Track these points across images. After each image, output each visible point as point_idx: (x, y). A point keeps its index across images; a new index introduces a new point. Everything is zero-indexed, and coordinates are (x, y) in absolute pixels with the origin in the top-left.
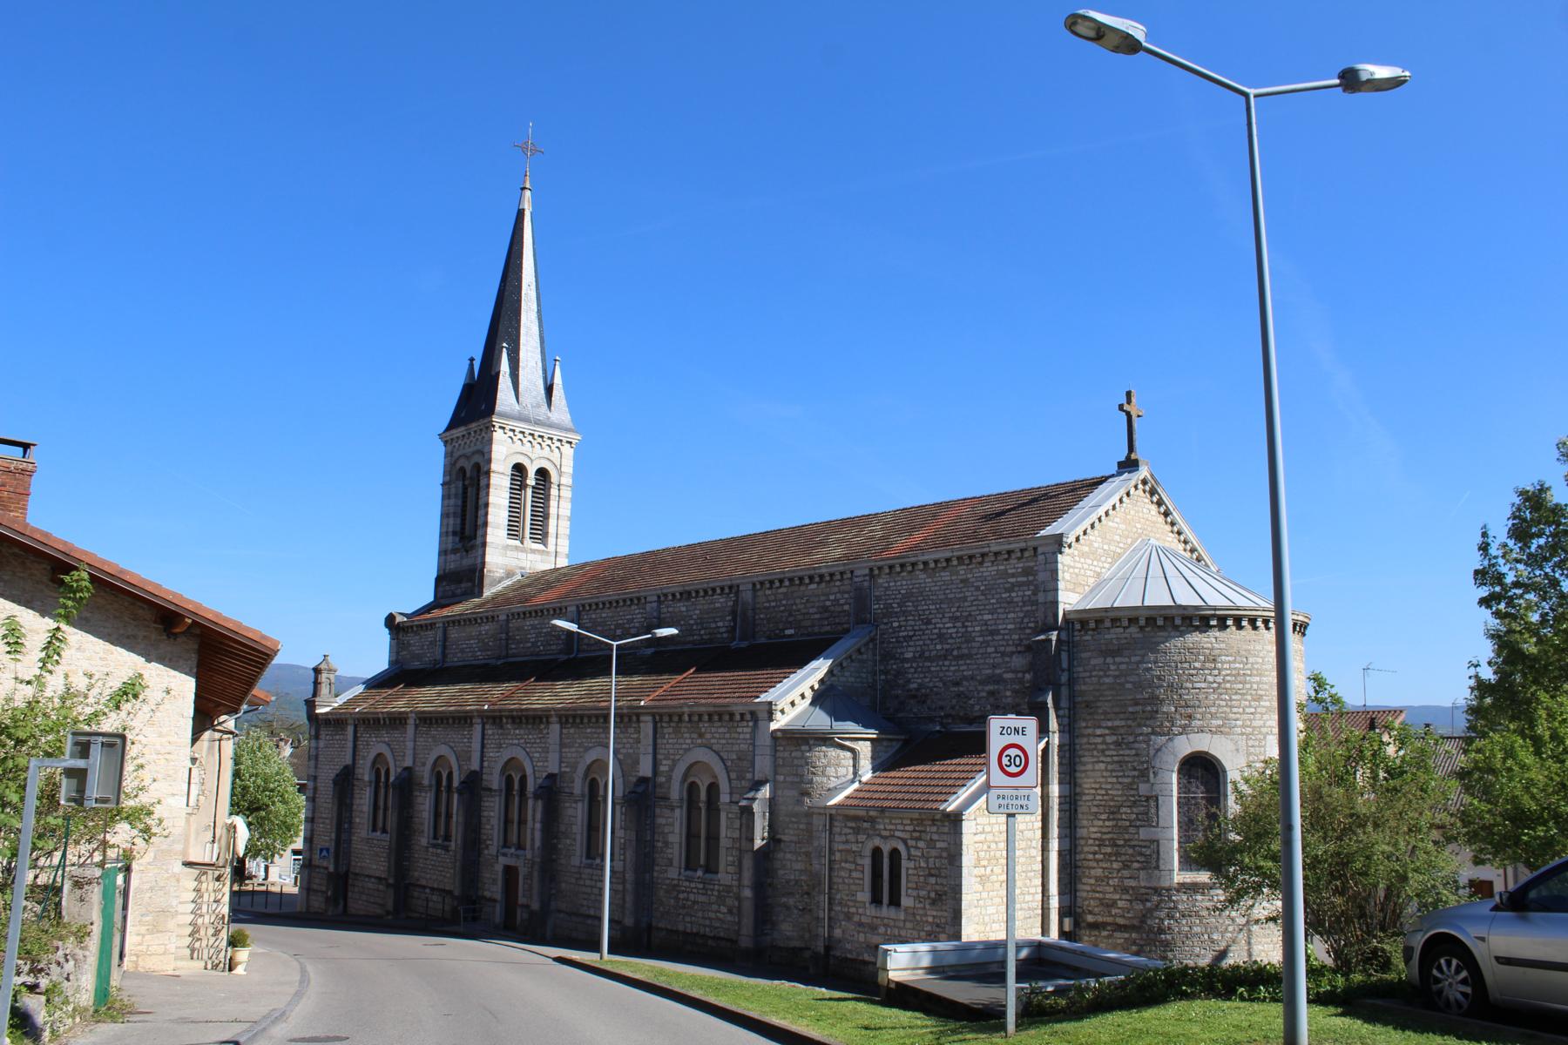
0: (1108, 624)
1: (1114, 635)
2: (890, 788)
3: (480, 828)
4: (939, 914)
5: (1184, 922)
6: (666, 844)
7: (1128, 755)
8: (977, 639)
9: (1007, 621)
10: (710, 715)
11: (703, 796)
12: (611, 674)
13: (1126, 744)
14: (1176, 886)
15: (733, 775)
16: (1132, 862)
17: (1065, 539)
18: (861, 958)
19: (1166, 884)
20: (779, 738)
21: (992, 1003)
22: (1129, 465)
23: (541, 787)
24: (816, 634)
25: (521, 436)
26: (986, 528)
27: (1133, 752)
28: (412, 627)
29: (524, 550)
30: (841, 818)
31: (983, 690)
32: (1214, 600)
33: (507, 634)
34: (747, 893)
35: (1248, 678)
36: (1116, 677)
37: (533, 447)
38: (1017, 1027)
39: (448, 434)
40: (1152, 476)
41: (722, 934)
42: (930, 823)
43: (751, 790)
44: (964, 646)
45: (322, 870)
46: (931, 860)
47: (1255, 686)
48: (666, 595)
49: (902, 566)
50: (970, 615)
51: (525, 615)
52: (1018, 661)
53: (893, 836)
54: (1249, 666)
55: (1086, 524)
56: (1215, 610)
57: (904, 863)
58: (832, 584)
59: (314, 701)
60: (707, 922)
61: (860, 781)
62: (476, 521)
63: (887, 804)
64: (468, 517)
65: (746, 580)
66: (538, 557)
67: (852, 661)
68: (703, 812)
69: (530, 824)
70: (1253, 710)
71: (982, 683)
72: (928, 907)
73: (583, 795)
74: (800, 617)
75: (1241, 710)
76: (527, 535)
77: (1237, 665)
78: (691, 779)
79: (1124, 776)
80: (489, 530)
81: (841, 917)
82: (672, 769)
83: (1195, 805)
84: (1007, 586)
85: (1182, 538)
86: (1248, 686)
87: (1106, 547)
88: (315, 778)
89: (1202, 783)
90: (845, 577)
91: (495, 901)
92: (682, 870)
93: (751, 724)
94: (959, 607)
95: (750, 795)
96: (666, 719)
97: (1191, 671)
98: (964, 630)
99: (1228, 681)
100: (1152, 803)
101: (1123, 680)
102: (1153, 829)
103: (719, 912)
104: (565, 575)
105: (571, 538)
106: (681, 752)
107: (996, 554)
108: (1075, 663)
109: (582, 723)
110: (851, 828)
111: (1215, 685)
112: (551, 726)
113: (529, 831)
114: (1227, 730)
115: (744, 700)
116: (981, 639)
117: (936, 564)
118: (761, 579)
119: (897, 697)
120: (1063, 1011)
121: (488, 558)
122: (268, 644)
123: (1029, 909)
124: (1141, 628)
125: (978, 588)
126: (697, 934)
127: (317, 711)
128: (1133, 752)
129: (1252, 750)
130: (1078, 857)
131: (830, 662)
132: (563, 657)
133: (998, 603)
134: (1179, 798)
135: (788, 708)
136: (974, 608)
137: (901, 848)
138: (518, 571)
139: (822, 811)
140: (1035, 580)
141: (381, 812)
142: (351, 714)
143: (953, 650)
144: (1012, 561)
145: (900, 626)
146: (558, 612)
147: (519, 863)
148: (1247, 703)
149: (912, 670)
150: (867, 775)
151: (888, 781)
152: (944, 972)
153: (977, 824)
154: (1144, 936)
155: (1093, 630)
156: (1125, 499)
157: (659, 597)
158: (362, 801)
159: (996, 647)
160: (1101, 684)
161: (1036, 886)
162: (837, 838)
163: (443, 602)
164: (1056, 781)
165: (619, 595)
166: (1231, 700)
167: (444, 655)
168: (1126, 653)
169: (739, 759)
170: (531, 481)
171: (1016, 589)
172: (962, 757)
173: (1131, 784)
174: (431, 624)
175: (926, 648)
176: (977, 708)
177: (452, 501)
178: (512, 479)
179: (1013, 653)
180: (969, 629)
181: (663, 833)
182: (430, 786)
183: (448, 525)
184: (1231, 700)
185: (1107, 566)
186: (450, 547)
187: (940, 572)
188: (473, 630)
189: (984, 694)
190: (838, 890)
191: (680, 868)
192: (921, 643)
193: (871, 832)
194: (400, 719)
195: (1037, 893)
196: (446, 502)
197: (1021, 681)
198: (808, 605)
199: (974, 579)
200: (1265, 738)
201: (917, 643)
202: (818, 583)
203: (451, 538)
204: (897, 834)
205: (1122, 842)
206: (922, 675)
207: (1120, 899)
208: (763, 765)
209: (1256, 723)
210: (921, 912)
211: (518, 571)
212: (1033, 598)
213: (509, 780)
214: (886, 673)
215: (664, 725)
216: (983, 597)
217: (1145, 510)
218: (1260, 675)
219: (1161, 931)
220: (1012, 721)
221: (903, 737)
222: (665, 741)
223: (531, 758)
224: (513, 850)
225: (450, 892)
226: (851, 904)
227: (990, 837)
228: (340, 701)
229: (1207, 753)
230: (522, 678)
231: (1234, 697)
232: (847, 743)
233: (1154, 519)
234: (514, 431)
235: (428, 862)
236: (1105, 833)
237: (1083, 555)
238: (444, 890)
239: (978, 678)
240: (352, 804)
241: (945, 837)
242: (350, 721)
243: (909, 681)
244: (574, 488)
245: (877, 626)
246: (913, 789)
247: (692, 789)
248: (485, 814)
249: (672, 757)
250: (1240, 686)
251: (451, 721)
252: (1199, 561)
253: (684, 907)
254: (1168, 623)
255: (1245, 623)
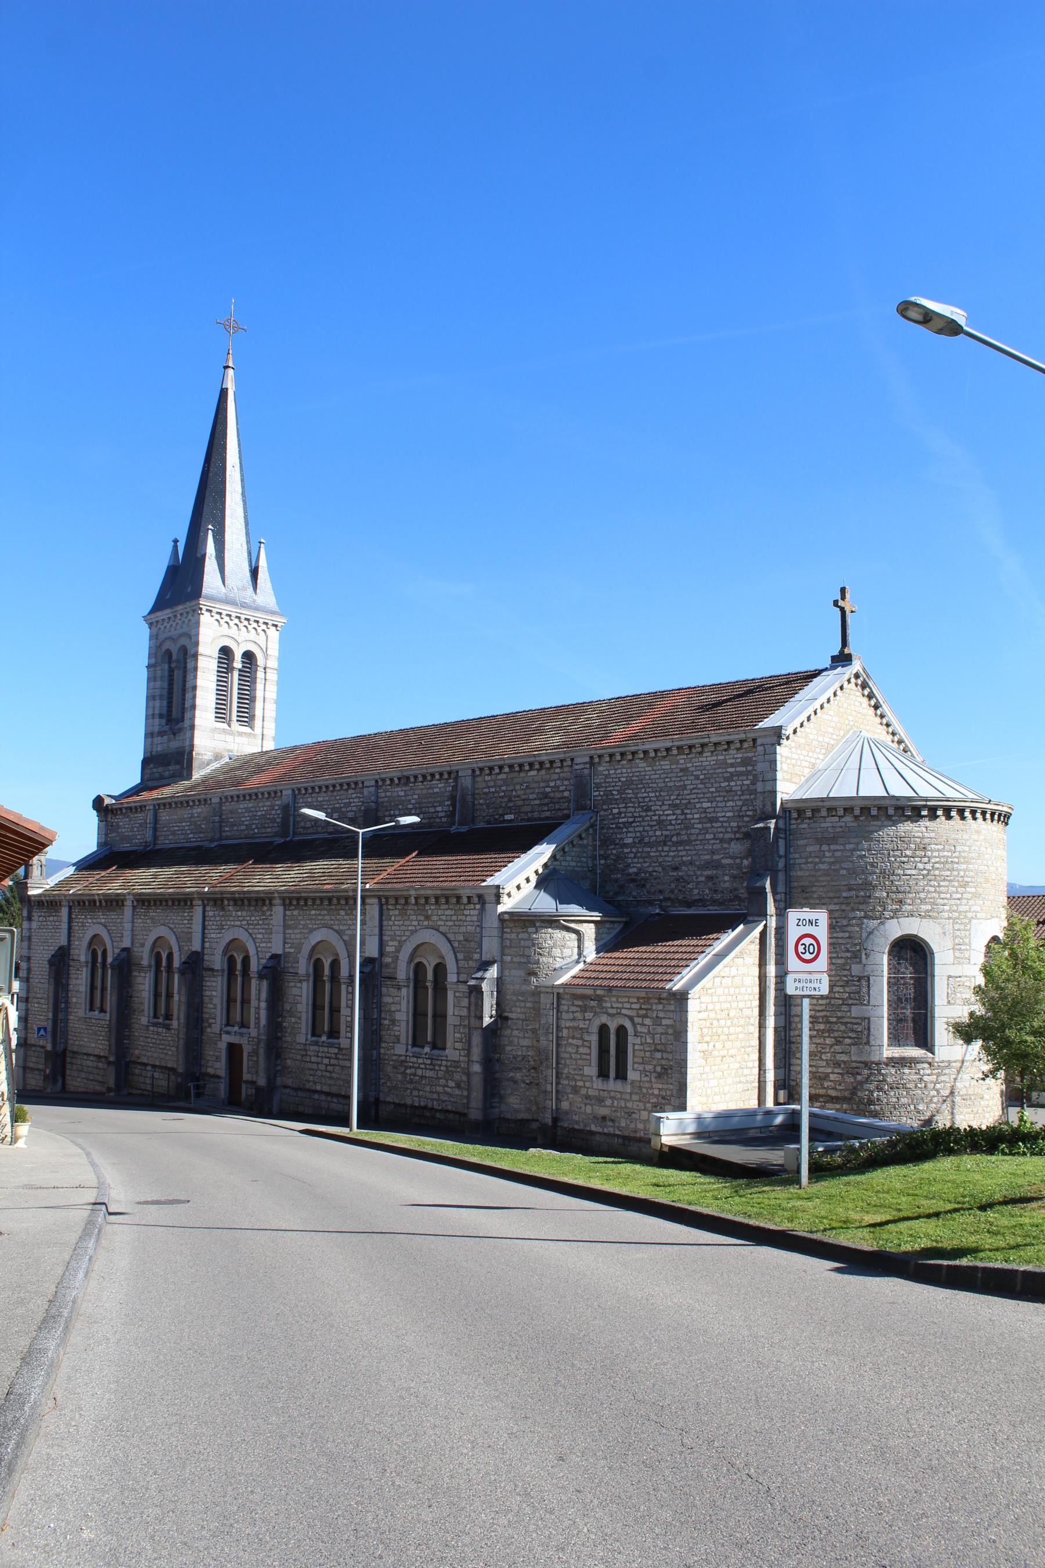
0: (824, 813)
1: (829, 823)
2: (615, 968)
3: (202, 1007)
4: (665, 1087)
5: (892, 1093)
6: (393, 1021)
7: (842, 938)
8: (696, 826)
9: (726, 809)
10: (437, 898)
11: (430, 976)
12: (357, 856)
13: (840, 927)
14: (885, 1060)
15: (460, 956)
16: (844, 1038)
17: (783, 732)
18: (588, 1129)
19: (876, 1059)
20: (506, 920)
21: (763, 1163)
22: (842, 659)
23: (265, 967)
24: (535, 819)
25: (227, 619)
26: (704, 718)
27: (847, 935)
28: (121, 809)
29: (231, 733)
30: (568, 997)
31: (702, 875)
32: (925, 791)
33: (220, 816)
34: (477, 1068)
35: (956, 866)
36: (832, 863)
37: (239, 630)
38: (809, 1179)
39: (153, 616)
40: (864, 670)
41: (449, 1108)
42: (656, 1001)
43: (479, 970)
44: (684, 832)
45: (38, 1049)
46: (657, 1036)
47: (962, 873)
48: (383, 780)
49: (622, 754)
50: (689, 803)
51: (239, 798)
52: (736, 848)
53: (620, 1014)
54: (957, 854)
55: (803, 717)
56: (927, 801)
57: (631, 1039)
58: (552, 771)
59: (26, 883)
60: (435, 1096)
61: (585, 962)
62: (184, 704)
63: (613, 983)
64: (174, 700)
65: (465, 766)
66: (244, 740)
67: (573, 846)
68: (430, 991)
69: (254, 1003)
70: (959, 896)
71: (702, 868)
72: (653, 1080)
73: (308, 975)
74: (520, 803)
75: (948, 896)
76: (234, 718)
77: (946, 853)
78: (156, 950)
79: (838, 957)
80: (198, 713)
81: (569, 1090)
82: (398, 950)
83: (904, 984)
84: (725, 775)
85: (890, 730)
86: (955, 873)
87: (820, 739)
88: (29, 959)
89: (911, 964)
90: (565, 764)
91: (219, 1077)
92: (410, 1047)
93: (478, 907)
94: (679, 795)
95: (479, 975)
96: (392, 901)
97: (903, 859)
98: (683, 817)
99: (937, 869)
100: (864, 983)
101: (837, 867)
102: (864, 1007)
103: (447, 1086)
104: (275, 758)
105: (277, 720)
106: (407, 933)
107: (716, 744)
108: (792, 850)
109: (306, 904)
110: (578, 1006)
111: (925, 872)
112: (274, 908)
113: (253, 1010)
114: (935, 914)
115: (471, 884)
116: (700, 826)
117: (656, 753)
118: (480, 765)
119: (617, 880)
120: (839, 1167)
121: (197, 741)
122: (47, 835)
123: (747, 1082)
124: (856, 817)
125: (697, 777)
126: (425, 1108)
127: (30, 893)
128: (847, 935)
129: (958, 933)
130: (792, 1034)
131: (554, 846)
132: (280, 840)
133: (717, 791)
134: (889, 978)
135: (514, 891)
136: (694, 796)
137: (628, 1025)
138: (226, 754)
139: (549, 990)
140: (754, 770)
141: (98, 993)
142: (65, 896)
143: (673, 836)
144: (731, 752)
145: (620, 813)
146: (273, 795)
147: (243, 1041)
148: (954, 889)
149: (632, 855)
150: (590, 953)
151: (612, 961)
152: (709, 1137)
153: (701, 1003)
154: (855, 1107)
155: (809, 818)
156: (839, 692)
157: (377, 781)
158: (78, 982)
159: (714, 834)
160: (817, 871)
161: (753, 1061)
162: (564, 1016)
163: (150, 784)
164: (773, 962)
165: (336, 779)
166: (939, 886)
167: (155, 837)
168: (841, 840)
169: (466, 940)
170: (238, 664)
171: (735, 778)
172: (683, 939)
173: (844, 964)
174: (141, 807)
175: (645, 834)
176: (696, 891)
177: (158, 684)
178: (219, 662)
179: (731, 840)
180: (689, 816)
181: (389, 1011)
182: (150, 966)
183: (154, 708)
184: (939, 886)
185: (821, 757)
186: (156, 729)
187: (659, 761)
188: (185, 813)
189: (703, 879)
190: (565, 1065)
191: (407, 1044)
192: (641, 829)
193: (598, 1010)
194: (117, 901)
195: (753, 1067)
196: (152, 684)
197: (739, 867)
198: (528, 791)
199: (693, 769)
200: (970, 922)
201: (637, 829)
202: (538, 770)
203: (157, 721)
204: (624, 1011)
205: (835, 1020)
206: (641, 860)
207: (833, 1073)
208: (490, 946)
209: (961, 908)
210: (647, 1085)
211: (226, 754)
212: (752, 787)
213: (231, 961)
214: (605, 857)
215: (390, 907)
216: (702, 786)
217: (857, 703)
218: (967, 863)
219: (871, 1102)
220: (806, 914)
221: (624, 919)
222: (391, 923)
223: (254, 939)
224: (236, 1028)
225: (173, 1070)
226: (578, 1078)
227: (712, 1015)
228: (52, 882)
229: (916, 936)
230: (240, 860)
231: (942, 883)
232: (573, 925)
233: (865, 711)
234: (220, 614)
235: (149, 1040)
236: (819, 1011)
237: (799, 746)
238: (166, 1068)
239: (697, 863)
240: (68, 985)
241: (671, 1015)
242: (64, 903)
243: (628, 866)
244: (280, 671)
245: (598, 812)
246: (637, 969)
247: (419, 969)
248: (208, 993)
249: (398, 938)
250: (948, 873)
251: (170, 903)
252: (906, 752)
253: (411, 1082)
254: (881, 813)
255: (953, 813)
